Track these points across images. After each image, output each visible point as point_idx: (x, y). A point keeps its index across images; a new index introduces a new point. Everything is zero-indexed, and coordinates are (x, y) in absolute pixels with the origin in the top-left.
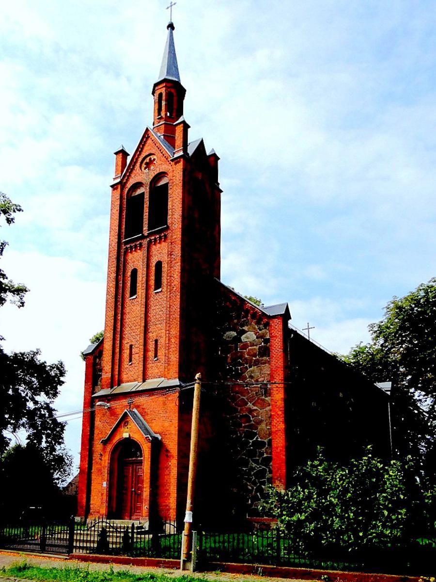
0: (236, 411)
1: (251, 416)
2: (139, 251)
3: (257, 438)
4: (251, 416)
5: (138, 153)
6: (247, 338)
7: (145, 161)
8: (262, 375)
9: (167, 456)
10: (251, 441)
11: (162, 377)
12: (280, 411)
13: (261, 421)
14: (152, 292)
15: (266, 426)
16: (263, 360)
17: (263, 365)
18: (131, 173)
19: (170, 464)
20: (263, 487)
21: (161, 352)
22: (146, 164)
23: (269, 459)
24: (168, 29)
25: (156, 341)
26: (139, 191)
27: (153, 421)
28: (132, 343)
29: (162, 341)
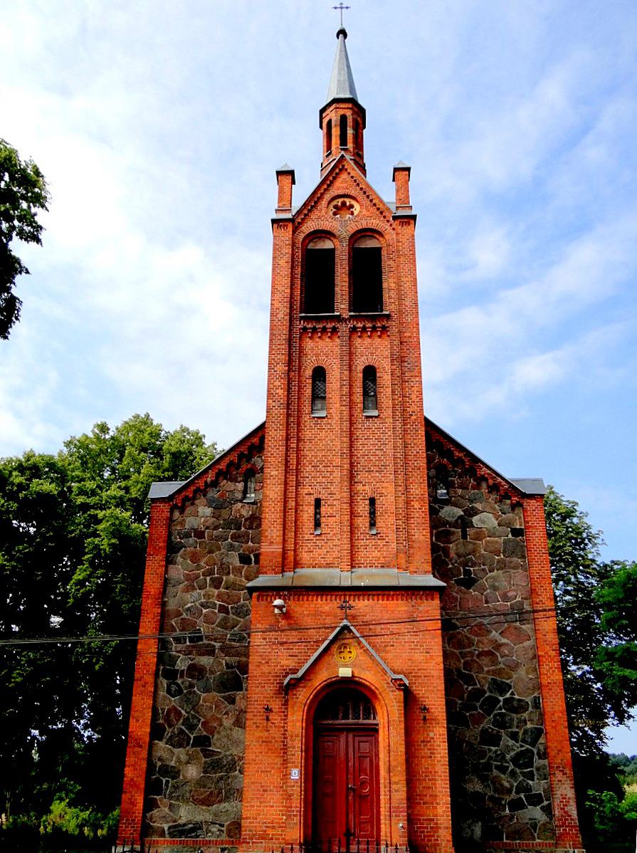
0: (471, 643)
1: (498, 654)
2: (328, 340)
3: (512, 694)
4: (498, 654)
5: (325, 186)
6: (483, 522)
7: (335, 203)
8: (513, 587)
9: (425, 719)
10: (501, 698)
11: (394, 566)
12: (553, 650)
13: (517, 665)
14: (359, 415)
15: (528, 673)
16: (511, 562)
17: (514, 571)
18: (310, 211)
19: (431, 735)
20: (531, 782)
21: (387, 522)
22: (343, 204)
23: (538, 733)
24: (338, 37)
25: (372, 502)
26: (328, 245)
27: (388, 648)
28: (320, 496)
29: (388, 502)
